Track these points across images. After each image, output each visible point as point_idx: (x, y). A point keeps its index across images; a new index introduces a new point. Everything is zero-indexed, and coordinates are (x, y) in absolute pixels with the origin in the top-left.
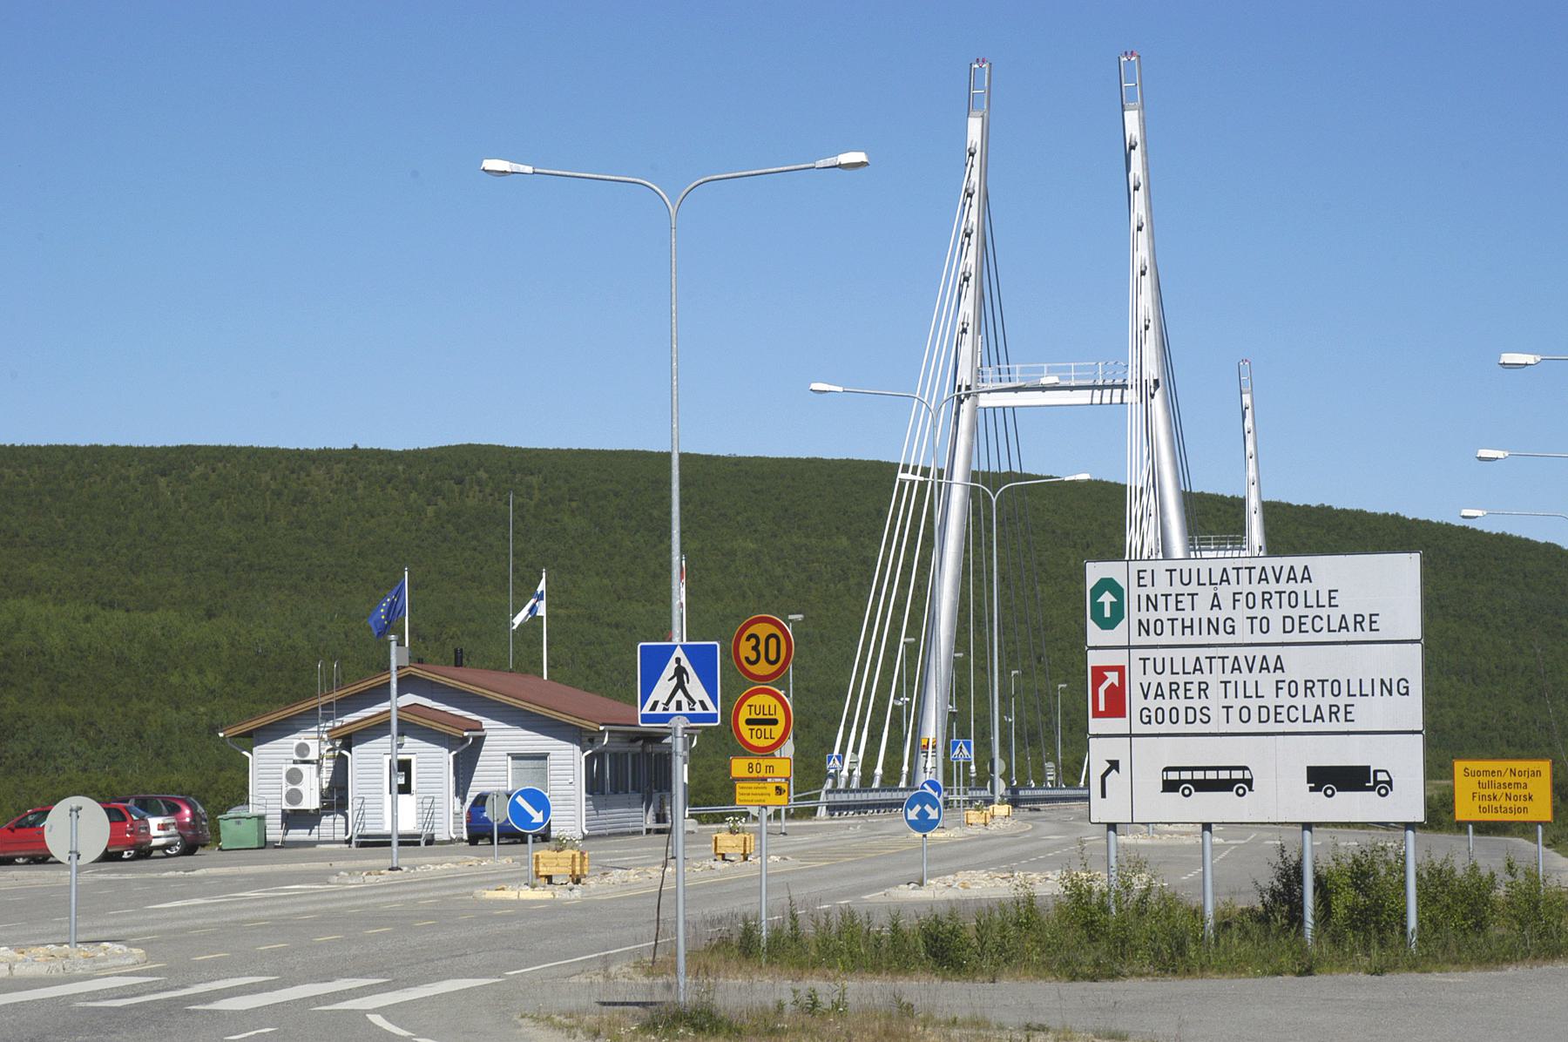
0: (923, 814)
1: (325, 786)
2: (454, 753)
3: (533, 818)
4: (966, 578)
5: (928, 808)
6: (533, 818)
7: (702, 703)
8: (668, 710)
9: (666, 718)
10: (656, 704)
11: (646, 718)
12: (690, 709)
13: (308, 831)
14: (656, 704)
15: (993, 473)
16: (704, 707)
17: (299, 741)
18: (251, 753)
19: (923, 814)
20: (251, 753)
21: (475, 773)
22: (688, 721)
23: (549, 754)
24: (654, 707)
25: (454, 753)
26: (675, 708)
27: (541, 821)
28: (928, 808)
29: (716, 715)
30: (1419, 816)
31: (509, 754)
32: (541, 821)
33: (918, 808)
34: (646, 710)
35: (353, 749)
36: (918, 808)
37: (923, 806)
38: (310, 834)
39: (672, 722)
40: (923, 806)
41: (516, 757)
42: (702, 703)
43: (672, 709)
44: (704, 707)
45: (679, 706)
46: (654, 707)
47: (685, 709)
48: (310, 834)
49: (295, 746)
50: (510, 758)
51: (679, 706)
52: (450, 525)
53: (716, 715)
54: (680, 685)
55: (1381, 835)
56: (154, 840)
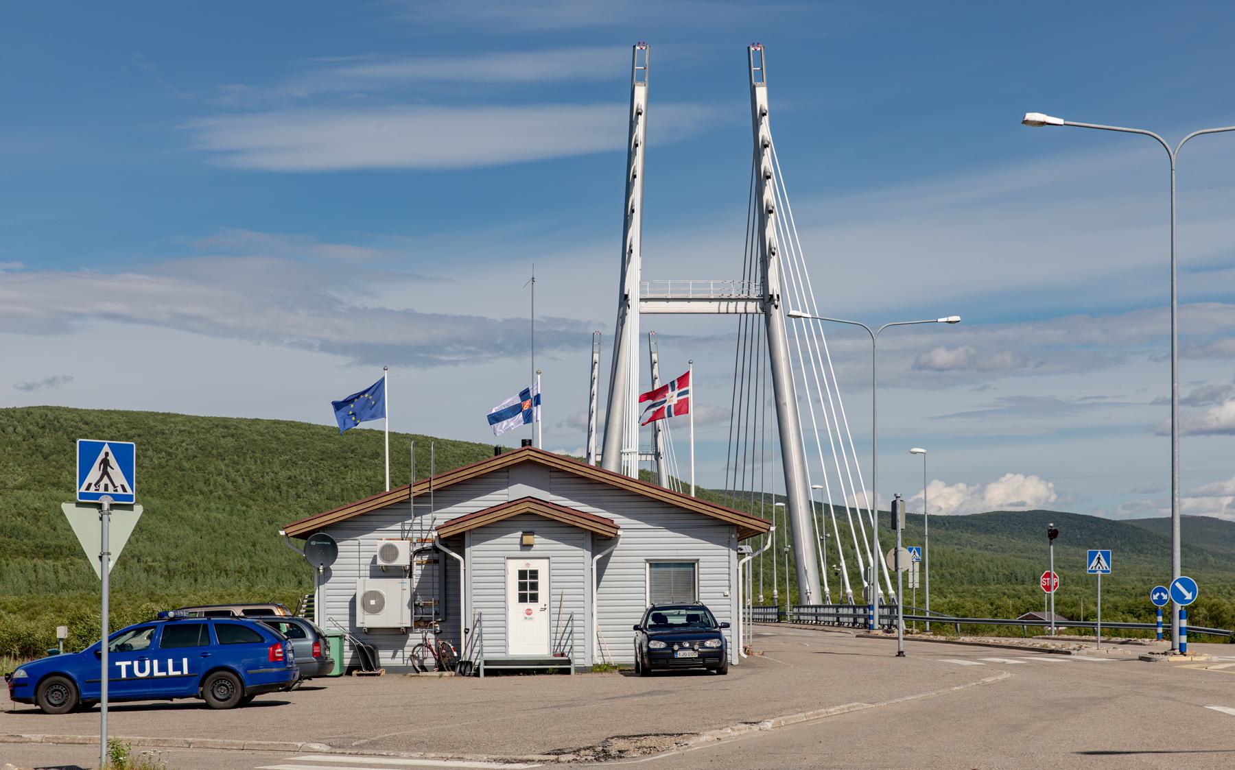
0: (1160, 597)
1: (415, 585)
2: (599, 557)
3: (1185, 597)
4: (842, 517)
5: (1162, 594)
6: (1185, 597)
7: (123, 486)
8: (98, 490)
9: (1095, 571)
10: (90, 485)
11: (1090, 571)
12: (115, 491)
13: (392, 653)
14: (90, 485)
15: (754, 493)
16: (124, 490)
17: (385, 542)
18: (462, 554)
19: (1160, 597)
20: (462, 554)
21: (607, 570)
22: (112, 499)
23: (698, 560)
24: (88, 488)
25: (599, 557)
26: (103, 490)
27: (1191, 598)
28: (1162, 594)
29: (132, 495)
30: (358, 625)
31: (647, 561)
32: (1191, 598)
33: (1158, 594)
34: (1090, 569)
35: (467, 550)
36: (1158, 594)
37: (1160, 593)
38: (394, 657)
39: (1097, 573)
40: (1160, 593)
41: (654, 564)
42: (123, 486)
43: (1097, 569)
44: (124, 490)
45: (1099, 568)
46: (88, 488)
47: (1101, 568)
48: (394, 657)
49: (378, 548)
50: (648, 565)
51: (1099, 568)
52: (195, 431)
53: (132, 495)
54: (105, 473)
55: (587, 678)
56: (576, 660)
